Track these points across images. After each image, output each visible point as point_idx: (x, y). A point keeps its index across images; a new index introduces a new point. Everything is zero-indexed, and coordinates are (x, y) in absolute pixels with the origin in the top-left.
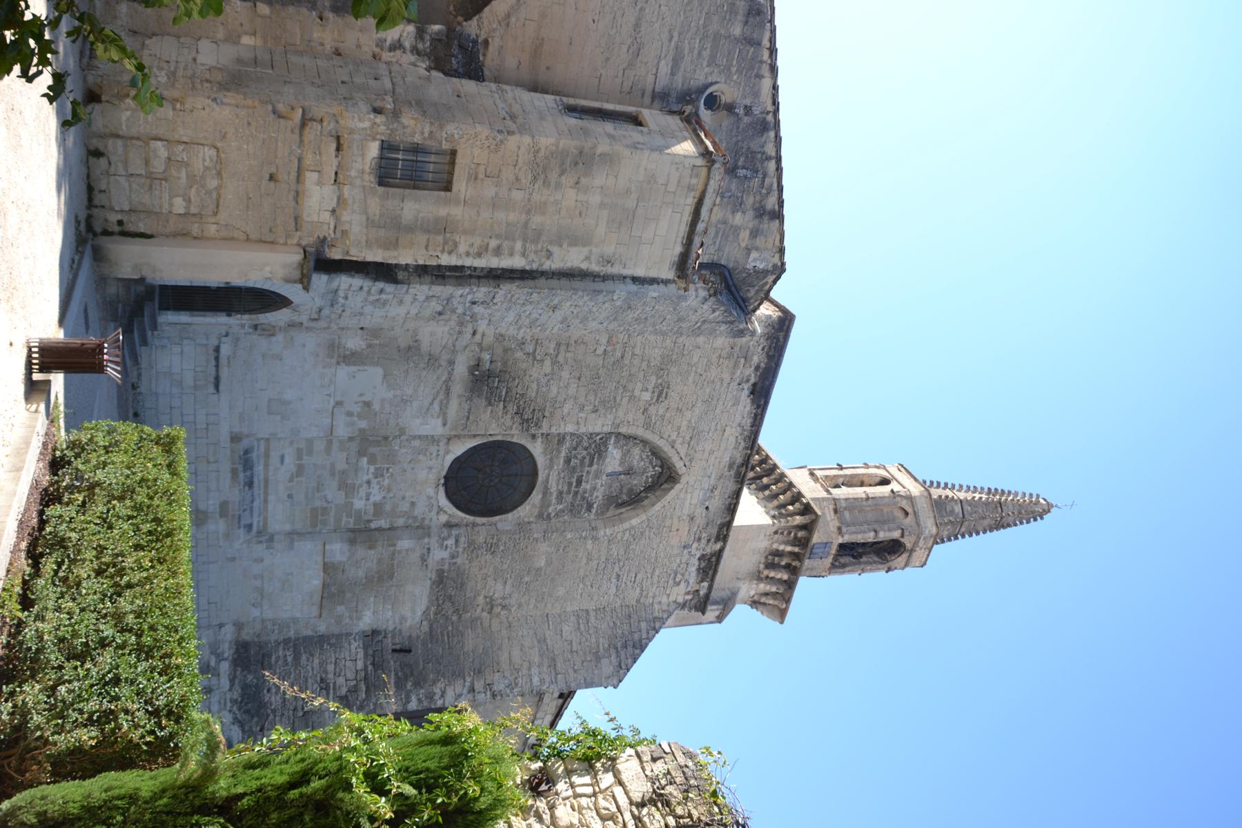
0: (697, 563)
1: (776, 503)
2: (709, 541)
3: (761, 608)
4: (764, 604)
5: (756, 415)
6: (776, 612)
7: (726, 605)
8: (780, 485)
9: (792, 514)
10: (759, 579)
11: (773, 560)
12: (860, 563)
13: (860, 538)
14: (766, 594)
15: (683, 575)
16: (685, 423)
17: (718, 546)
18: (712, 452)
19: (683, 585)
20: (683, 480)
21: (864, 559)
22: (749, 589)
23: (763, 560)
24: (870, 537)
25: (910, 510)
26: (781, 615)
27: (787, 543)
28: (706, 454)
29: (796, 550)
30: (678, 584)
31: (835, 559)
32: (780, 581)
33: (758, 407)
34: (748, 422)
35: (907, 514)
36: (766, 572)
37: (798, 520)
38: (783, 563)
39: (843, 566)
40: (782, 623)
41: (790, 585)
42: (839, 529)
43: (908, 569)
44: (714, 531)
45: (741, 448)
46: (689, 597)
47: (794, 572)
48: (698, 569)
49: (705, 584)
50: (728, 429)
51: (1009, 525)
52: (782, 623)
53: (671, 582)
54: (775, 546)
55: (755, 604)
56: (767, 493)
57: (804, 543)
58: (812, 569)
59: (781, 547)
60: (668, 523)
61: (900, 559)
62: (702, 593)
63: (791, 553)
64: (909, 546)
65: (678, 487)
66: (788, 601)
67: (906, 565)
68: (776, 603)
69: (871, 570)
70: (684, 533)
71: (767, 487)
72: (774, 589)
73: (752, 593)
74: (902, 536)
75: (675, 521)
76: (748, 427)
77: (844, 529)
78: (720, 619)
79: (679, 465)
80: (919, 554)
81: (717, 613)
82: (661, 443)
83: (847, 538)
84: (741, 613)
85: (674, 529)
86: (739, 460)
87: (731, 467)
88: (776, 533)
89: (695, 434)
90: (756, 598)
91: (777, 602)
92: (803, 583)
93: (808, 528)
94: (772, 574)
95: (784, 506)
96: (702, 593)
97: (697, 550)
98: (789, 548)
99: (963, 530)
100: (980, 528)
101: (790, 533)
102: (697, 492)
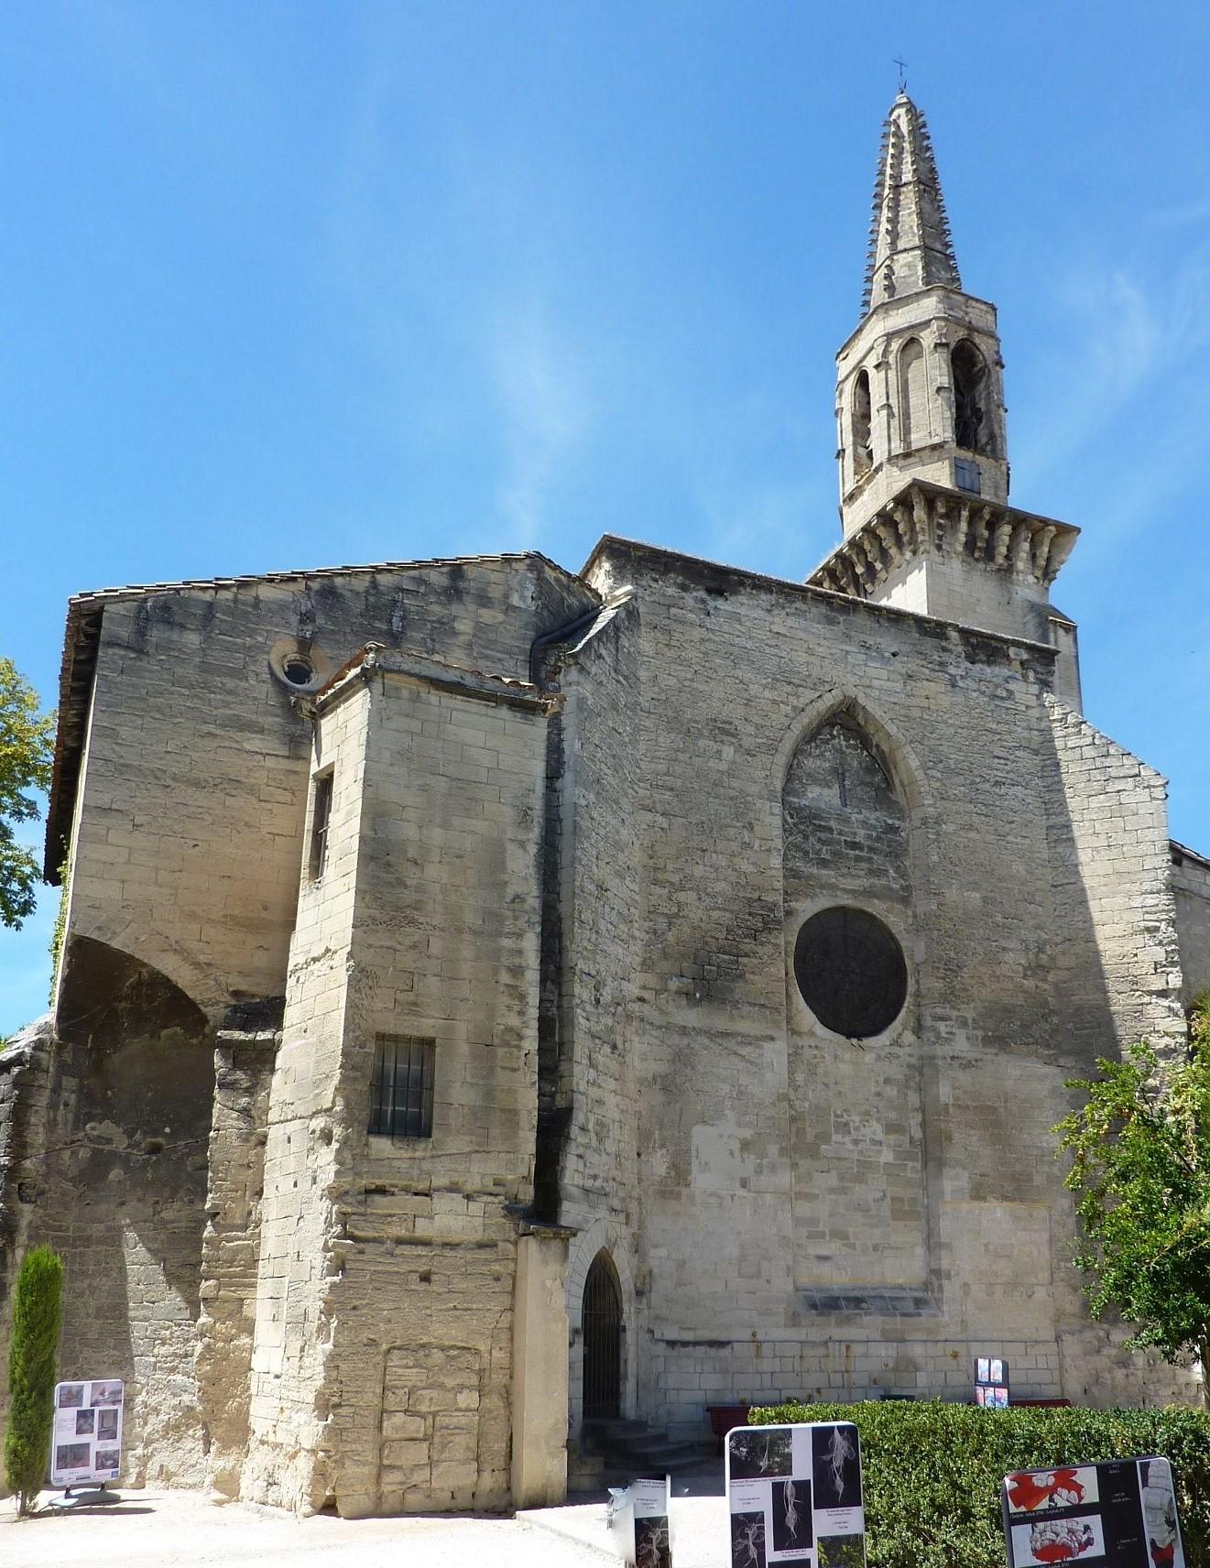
0: (979, 666)
1: (893, 551)
2: (945, 650)
3: (1054, 565)
4: (1049, 560)
5: (754, 587)
6: (1061, 540)
7: (1047, 618)
8: (867, 546)
9: (912, 524)
10: (1007, 572)
11: (980, 550)
12: (988, 411)
14: (1034, 557)
15: (997, 686)
16: (767, 694)
17: (954, 635)
18: (810, 652)
19: (1012, 686)
20: (852, 692)
21: (982, 405)
22: (1026, 586)
23: (981, 566)
25: (907, 336)
26: (1066, 532)
27: (955, 529)
28: (813, 659)
29: (965, 514)
30: (1011, 693)
31: (982, 452)
32: (1013, 536)
33: (742, 584)
34: (765, 599)
36: (1000, 560)
37: (919, 513)
38: (986, 533)
39: (992, 437)
40: (1078, 530)
41: (1020, 521)
43: (1000, 333)
44: (929, 644)
45: (804, 607)
46: (1031, 675)
47: (1000, 515)
48: (989, 663)
49: (1012, 651)
50: (775, 628)
51: (933, 170)
52: (1078, 530)
53: (1007, 704)
54: (960, 549)
55: (1048, 574)
56: (878, 566)
58: (997, 488)
59: (962, 538)
60: (916, 713)
61: (983, 347)
62: (1025, 656)
63: (971, 523)
64: (962, 334)
65: (862, 700)
66: (1045, 522)
67: (992, 335)
68: (1047, 542)
69: (1000, 392)
70: (934, 689)
72: (1026, 546)
73: (1031, 579)
75: (914, 701)
76: (773, 598)
78: (1070, 629)
79: (829, 700)
80: (976, 315)
81: (1061, 632)
82: (797, 729)
84: (1061, 595)
85: (925, 703)
86: (823, 609)
87: (831, 622)
88: (939, 548)
89: (785, 677)
90: (1039, 573)
91: (1046, 538)
92: (1017, 500)
94: (1003, 550)
95: (898, 538)
96: (1025, 656)
97: (958, 667)
98: (964, 526)
99: (938, 247)
100: (936, 217)
101: (939, 526)
102: (872, 672)
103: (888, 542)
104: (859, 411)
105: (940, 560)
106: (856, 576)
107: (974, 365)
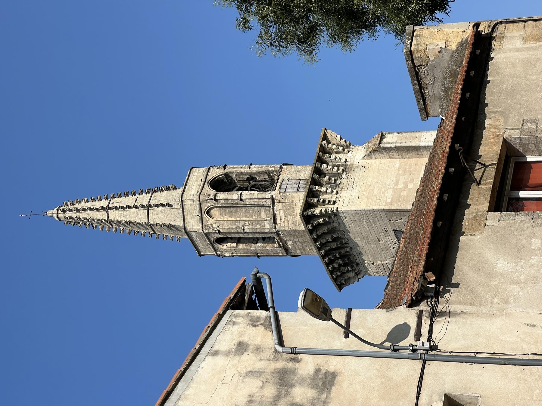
1: (331, 226)
8: (324, 241)
9: (321, 215)
13: (255, 194)
24: (246, 194)
35: (208, 213)
42: (273, 203)
57: (311, 194)
61: (215, 175)
71: (334, 240)
74: (216, 195)
77: (269, 202)
81: (384, 140)
83: (268, 195)
93: (308, 206)
103: (325, 229)
104: (261, 240)
105: (341, 202)
106: (337, 248)
107: (222, 180)
